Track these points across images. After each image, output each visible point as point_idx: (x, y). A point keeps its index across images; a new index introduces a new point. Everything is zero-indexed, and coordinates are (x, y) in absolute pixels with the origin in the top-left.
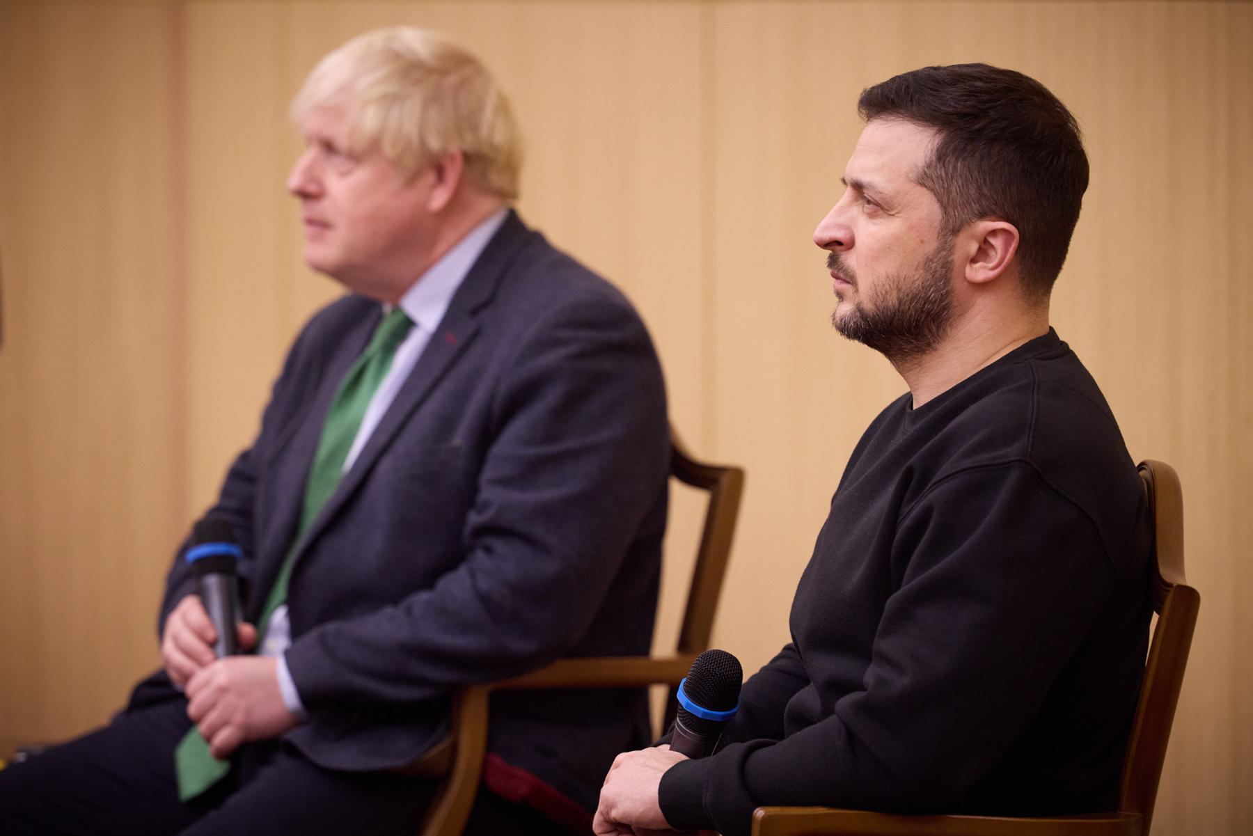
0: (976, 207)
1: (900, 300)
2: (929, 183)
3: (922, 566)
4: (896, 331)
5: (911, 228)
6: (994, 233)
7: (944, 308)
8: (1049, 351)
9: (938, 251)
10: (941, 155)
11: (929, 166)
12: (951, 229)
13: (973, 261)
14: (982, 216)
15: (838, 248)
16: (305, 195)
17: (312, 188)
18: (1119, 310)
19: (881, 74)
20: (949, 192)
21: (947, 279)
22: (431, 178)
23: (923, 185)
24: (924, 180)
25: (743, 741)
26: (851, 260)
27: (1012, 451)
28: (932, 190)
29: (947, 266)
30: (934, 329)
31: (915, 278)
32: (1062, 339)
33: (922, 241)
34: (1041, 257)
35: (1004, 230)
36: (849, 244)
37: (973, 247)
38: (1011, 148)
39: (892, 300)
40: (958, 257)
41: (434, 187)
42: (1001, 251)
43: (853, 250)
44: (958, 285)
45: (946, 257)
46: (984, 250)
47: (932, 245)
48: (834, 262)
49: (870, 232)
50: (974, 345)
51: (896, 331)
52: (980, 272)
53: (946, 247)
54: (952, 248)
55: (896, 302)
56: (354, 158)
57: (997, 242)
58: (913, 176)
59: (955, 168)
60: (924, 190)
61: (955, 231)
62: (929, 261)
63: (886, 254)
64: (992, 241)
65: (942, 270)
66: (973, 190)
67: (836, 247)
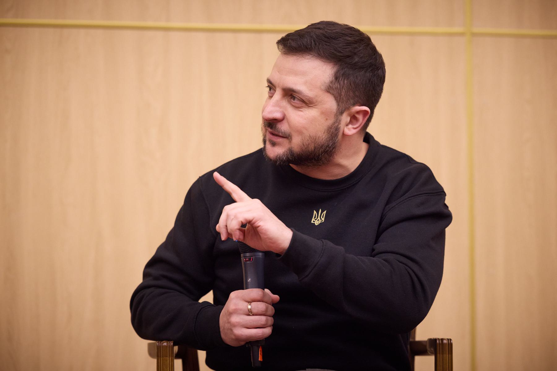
0: (352, 101)
1: (315, 148)
2: (331, 91)
6: (358, 112)
9: (334, 123)
10: (337, 77)
11: (331, 82)
20: (340, 95)
24: (329, 90)
25: (274, 294)
26: (283, 127)
28: (333, 94)
29: (337, 129)
33: (327, 119)
39: (312, 147)
55: (313, 148)
57: (360, 117)
59: (344, 82)
60: (329, 95)
61: (342, 113)
64: (357, 116)
65: (334, 132)
66: (351, 94)
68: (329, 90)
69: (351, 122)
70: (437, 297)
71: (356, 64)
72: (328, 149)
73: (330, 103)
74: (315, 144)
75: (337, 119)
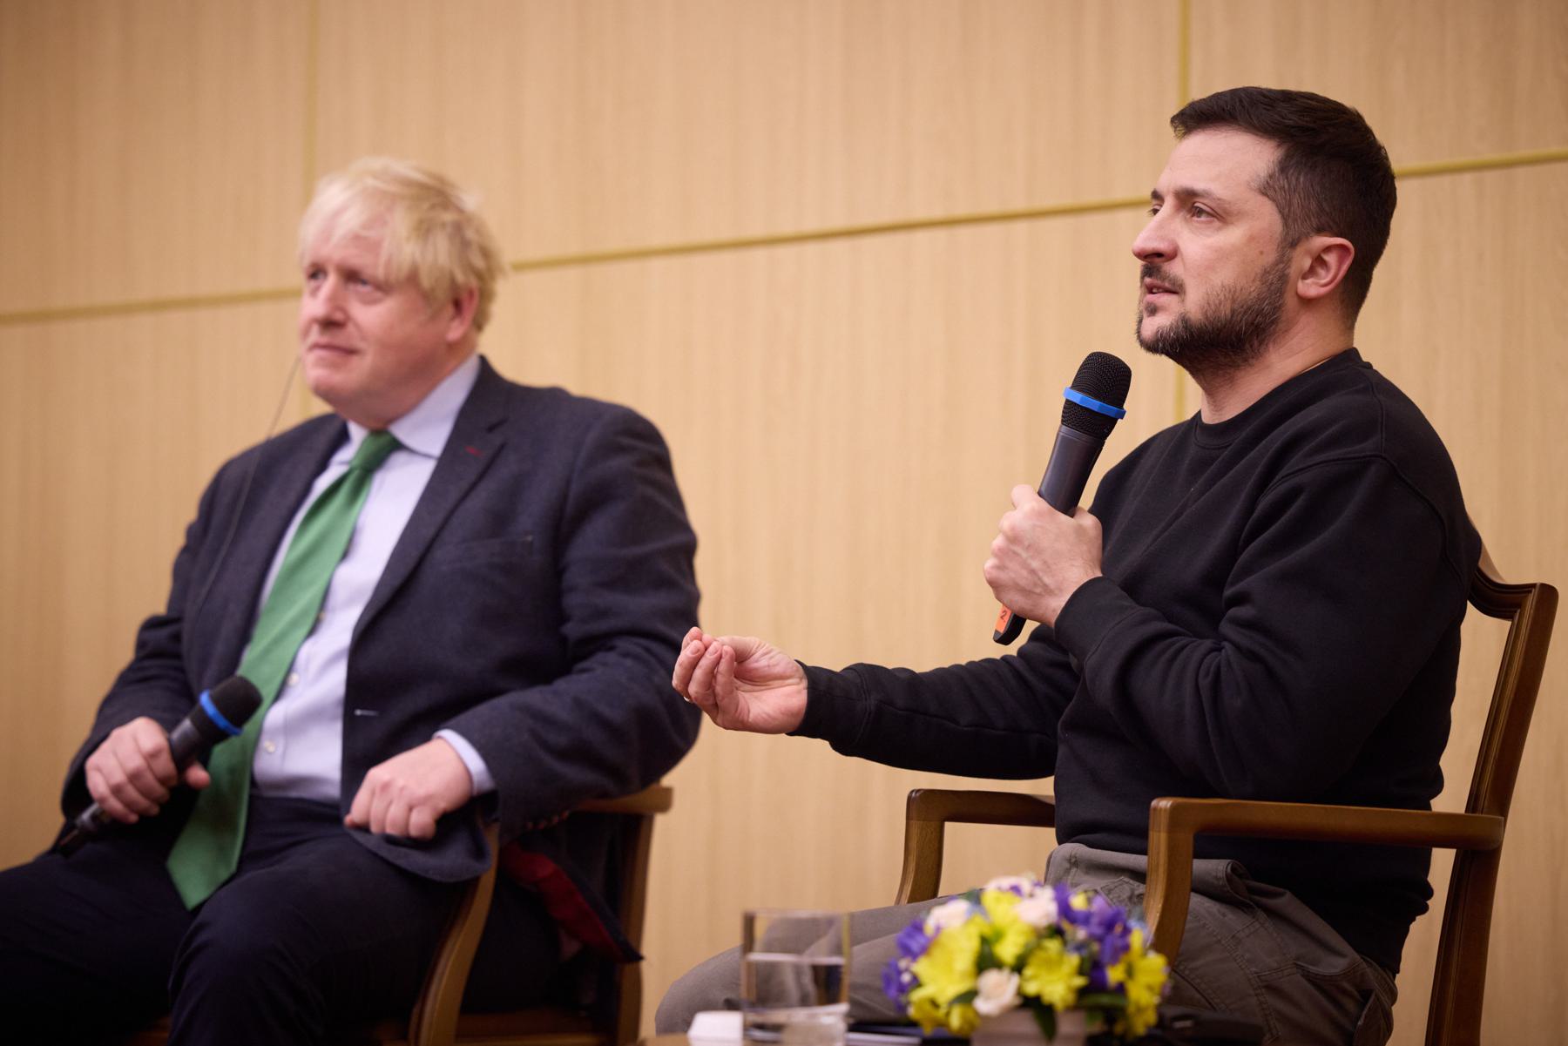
0: (1315, 222)
1: (1233, 312)
2: (1271, 193)
3: (1233, 584)
4: (1204, 348)
5: (1251, 239)
6: (1328, 249)
7: (1272, 322)
8: (1346, 370)
9: (1276, 263)
10: (1283, 167)
11: (1271, 177)
12: (1291, 243)
13: (1304, 277)
14: (1320, 231)
15: (1157, 260)
16: (329, 324)
17: (339, 316)
18: (1416, 333)
19: (1200, 91)
20: (1290, 205)
21: (1281, 292)
22: (450, 310)
23: (1264, 194)
24: (1266, 190)
25: (1424, 909)
26: (1175, 269)
27: (1368, 447)
29: (1283, 278)
30: (1256, 343)
31: (1253, 289)
32: (1365, 359)
34: (1354, 288)
35: (1342, 246)
36: (1172, 255)
37: (1307, 263)
38: (1336, 169)
39: (1225, 310)
40: (1293, 271)
41: (453, 319)
42: (1336, 267)
43: (1177, 260)
44: (1290, 301)
45: (1284, 269)
46: (1319, 261)
47: (1271, 257)
48: (1149, 271)
49: (1196, 245)
50: (1290, 358)
51: (1204, 348)
52: (1310, 288)
53: (1283, 260)
54: (1290, 260)
56: (383, 288)
57: (1331, 258)
58: (1254, 185)
61: (1294, 244)
62: (1266, 272)
63: (1213, 265)
64: (1327, 257)
65: (1276, 281)
66: (1313, 206)
67: (1154, 262)
68: (1266, 190)
69: (1311, 272)
70: (1404, 390)
71: (1336, 169)
72: (1259, 319)
73: (1265, 218)
74: (1234, 301)
75: (1283, 255)
